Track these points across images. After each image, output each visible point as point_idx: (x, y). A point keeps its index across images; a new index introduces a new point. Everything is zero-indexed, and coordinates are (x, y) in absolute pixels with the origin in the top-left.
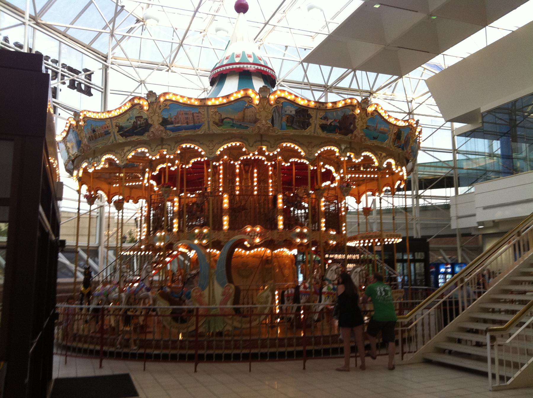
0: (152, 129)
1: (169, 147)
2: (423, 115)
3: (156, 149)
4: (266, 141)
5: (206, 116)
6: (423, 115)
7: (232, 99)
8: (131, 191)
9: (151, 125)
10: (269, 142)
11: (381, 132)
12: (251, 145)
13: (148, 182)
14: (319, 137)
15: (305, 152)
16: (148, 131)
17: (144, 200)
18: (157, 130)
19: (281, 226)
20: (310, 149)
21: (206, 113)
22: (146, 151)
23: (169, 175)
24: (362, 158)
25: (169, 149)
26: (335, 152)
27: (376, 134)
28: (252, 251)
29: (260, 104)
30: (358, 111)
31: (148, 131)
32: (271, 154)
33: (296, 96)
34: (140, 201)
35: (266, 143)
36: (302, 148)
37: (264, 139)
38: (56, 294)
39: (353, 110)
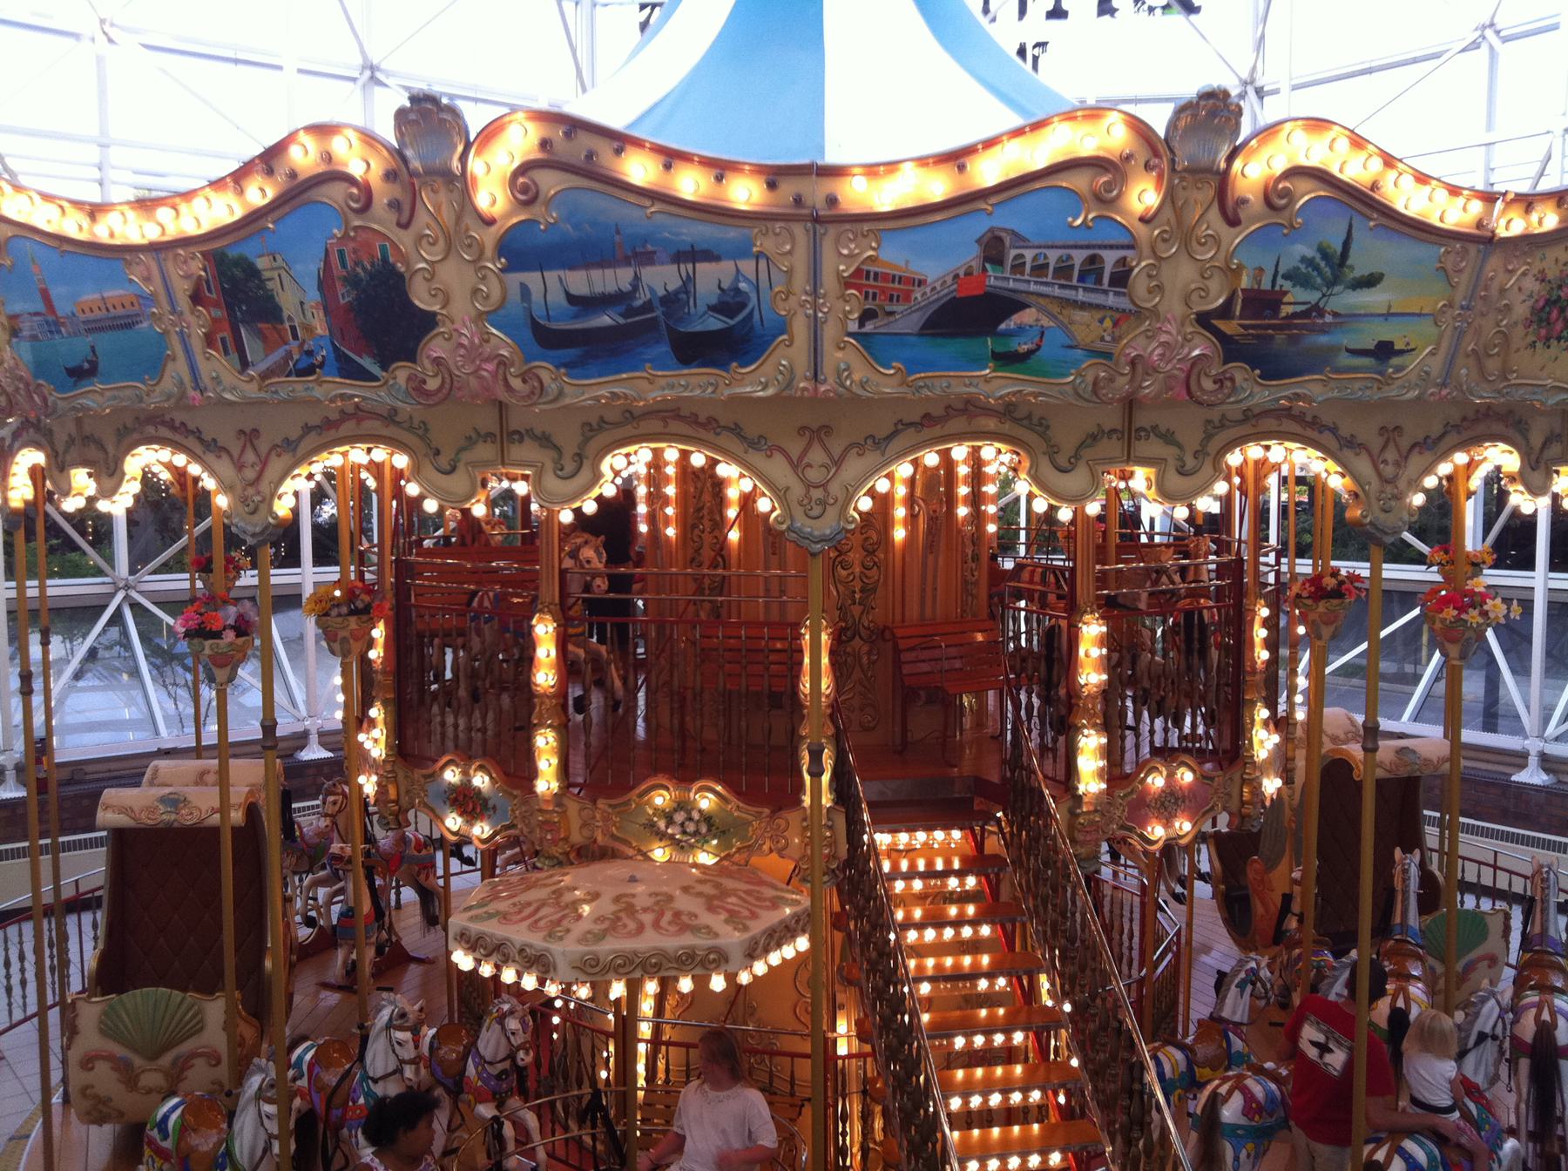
0: (436, 347)
1: (1169, 452)
2: (357, 37)
3: (466, 457)
5: (800, 281)
6: (357, 37)
7: (987, 172)
9: (428, 322)
10: (1168, 438)
11: (95, 327)
14: (852, 402)
16: (411, 357)
18: (473, 353)
21: (800, 262)
22: (401, 461)
25: (1172, 462)
27: (74, 348)
29: (1168, 213)
30: (1143, 196)
31: (411, 357)
32: (590, 507)
33: (1389, 161)
35: (1155, 447)
39: (1107, 199)
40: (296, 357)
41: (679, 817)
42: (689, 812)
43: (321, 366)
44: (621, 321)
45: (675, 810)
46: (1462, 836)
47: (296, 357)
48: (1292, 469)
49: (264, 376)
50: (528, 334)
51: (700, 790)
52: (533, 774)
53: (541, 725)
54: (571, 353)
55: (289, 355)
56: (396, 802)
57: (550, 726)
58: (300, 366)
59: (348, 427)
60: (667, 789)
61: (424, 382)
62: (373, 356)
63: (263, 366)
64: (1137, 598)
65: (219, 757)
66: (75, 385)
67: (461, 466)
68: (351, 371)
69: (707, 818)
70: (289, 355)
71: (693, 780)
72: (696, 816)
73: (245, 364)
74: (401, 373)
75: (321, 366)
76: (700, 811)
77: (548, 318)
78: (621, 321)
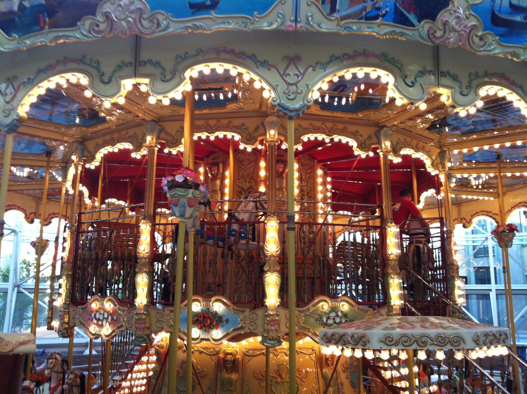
4: (150, 62)
8: (459, 210)
12: (106, 79)
13: (74, 186)
15: (274, 88)
17: (63, 222)
19: (272, 299)
20: (291, 79)
23: (108, 168)
24: (480, 104)
26: (81, 88)
28: (244, 343)
31: (433, 17)
34: (55, 221)
36: (263, 78)
37: (145, 56)
38: (157, 359)
40: (368, 10)
41: (333, 314)
42: (337, 313)
43: (383, 16)
44: (523, 21)
45: (330, 312)
46: (504, 288)
47: (368, 10)
48: (461, 159)
49: (343, 18)
50: (489, 18)
51: (217, 300)
52: (264, 295)
53: (141, 272)
54: (502, 30)
55: (365, 9)
56: (68, 324)
57: (145, 272)
58: (369, 15)
59: (360, 60)
60: (199, 301)
61: (436, 32)
62: (416, 14)
63: (344, 13)
64: (225, 228)
65: (510, 289)
66: (193, 14)
67: (417, 85)
68: (401, 19)
69: (345, 315)
70: (365, 9)
71: (212, 296)
72: (340, 314)
73: (333, 10)
74: (425, 26)
75: (383, 16)
76: (342, 312)
77: (500, 12)
78: (523, 21)
